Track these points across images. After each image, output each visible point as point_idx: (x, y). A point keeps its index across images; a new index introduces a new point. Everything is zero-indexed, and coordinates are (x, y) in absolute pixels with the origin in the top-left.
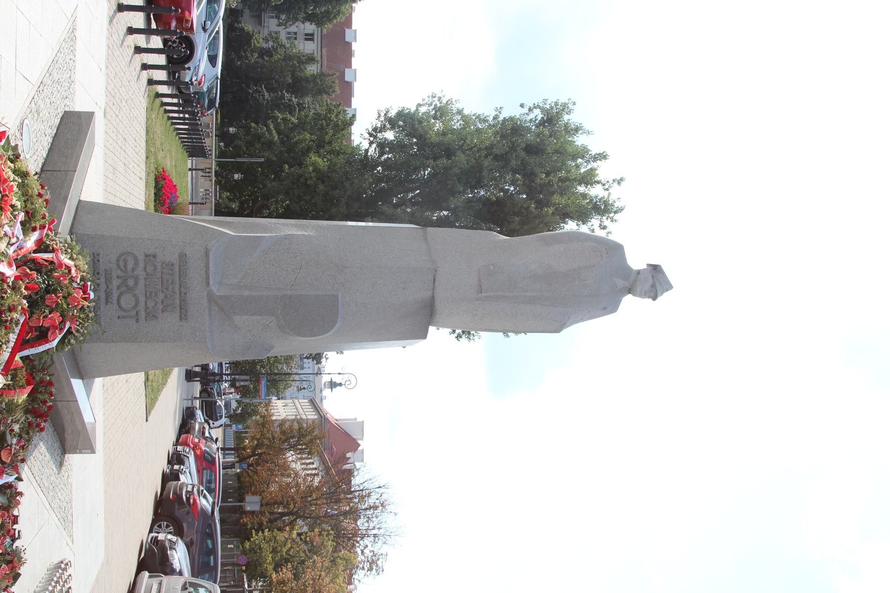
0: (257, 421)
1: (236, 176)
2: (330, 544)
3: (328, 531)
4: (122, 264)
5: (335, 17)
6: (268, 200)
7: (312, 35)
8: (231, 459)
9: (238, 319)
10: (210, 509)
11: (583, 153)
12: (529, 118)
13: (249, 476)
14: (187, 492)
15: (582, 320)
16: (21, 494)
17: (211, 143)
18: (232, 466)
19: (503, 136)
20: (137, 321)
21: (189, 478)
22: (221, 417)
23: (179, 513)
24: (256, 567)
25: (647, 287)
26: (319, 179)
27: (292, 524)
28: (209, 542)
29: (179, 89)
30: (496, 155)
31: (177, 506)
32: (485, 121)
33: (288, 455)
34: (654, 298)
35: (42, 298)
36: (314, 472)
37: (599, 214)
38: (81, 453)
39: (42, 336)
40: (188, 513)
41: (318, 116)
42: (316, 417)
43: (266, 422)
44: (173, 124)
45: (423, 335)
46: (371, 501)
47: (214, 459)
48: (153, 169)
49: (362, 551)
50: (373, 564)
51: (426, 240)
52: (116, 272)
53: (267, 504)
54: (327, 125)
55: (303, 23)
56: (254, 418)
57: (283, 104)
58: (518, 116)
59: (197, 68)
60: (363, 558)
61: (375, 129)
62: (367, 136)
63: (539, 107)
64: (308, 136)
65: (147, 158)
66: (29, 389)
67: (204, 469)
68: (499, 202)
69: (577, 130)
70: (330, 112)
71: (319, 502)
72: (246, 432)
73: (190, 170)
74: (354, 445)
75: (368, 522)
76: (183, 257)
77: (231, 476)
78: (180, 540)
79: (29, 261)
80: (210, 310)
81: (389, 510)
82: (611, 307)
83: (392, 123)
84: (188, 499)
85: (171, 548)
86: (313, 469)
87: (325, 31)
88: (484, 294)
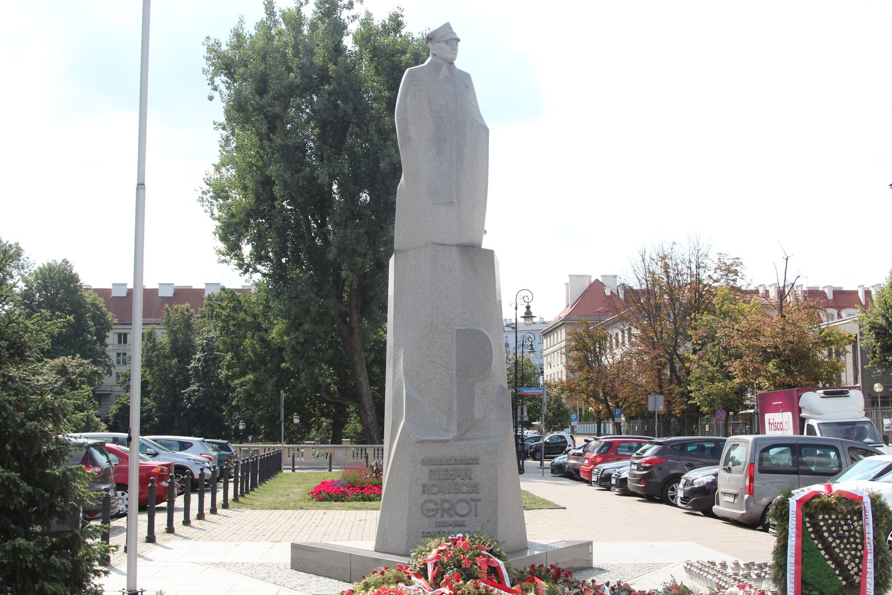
0: (568, 397)
1: (296, 421)
2: (706, 317)
3: (692, 319)
4: (431, 513)
5: (99, 309)
6: (320, 386)
7: (120, 335)
8: (610, 427)
9: (477, 416)
10: (656, 447)
11: (265, 28)
12: (226, 92)
13: (629, 407)
14: (638, 469)
15: (477, 107)
16: (619, 583)
17: (264, 448)
18: (618, 426)
19: (247, 121)
20: (479, 500)
21: (624, 469)
22: (562, 437)
23: (659, 478)
24: (729, 399)
25: (447, 48)
26: (297, 329)
27: (682, 360)
28: (689, 449)
29: (218, 480)
30: (269, 128)
31: (653, 480)
32: (227, 140)
33: (606, 363)
34: (459, 40)
35: (465, 570)
36: (626, 335)
37: (335, 10)
38: (591, 554)
39: (494, 571)
40: (660, 469)
41: (225, 330)
42: (563, 330)
43: (569, 388)
44: (201, 516)
45: (490, 254)
46: (659, 271)
47: (606, 443)
48: (311, 503)
49: (715, 281)
50: (729, 270)
51: (406, 250)
52: (438, 517)
53: (661, 387)
54: (234, 319)
55: (107, 346)
56: (564, 401)
57: (203, 368)
58: (224, 105)
59: (196, 462)
60: (722, 281)
61: (240, 266)
62: (247, 275)
63: (212, 79)
64: (247, 341)
65: (302, 508)
66: (537, 580)
67: (617, 454)
68: (323, 125)
69: (238, 36)
70: (219, 316)
71: (659, 329)
72: (581, 410)
73: (293, 470)
74: (597, 286)
75: (682, 275)
76: (424, 462)
77: (629, 426)
78: (686, 476)
79: (435, 582)
80: (469, 439)
81: (670, 251)
82: (465, 78)
83: (233, 248)
84: (645, 468)
85: (692, 485)
86: (623, 336)
87: (116, 321)
88: (455, 200)
